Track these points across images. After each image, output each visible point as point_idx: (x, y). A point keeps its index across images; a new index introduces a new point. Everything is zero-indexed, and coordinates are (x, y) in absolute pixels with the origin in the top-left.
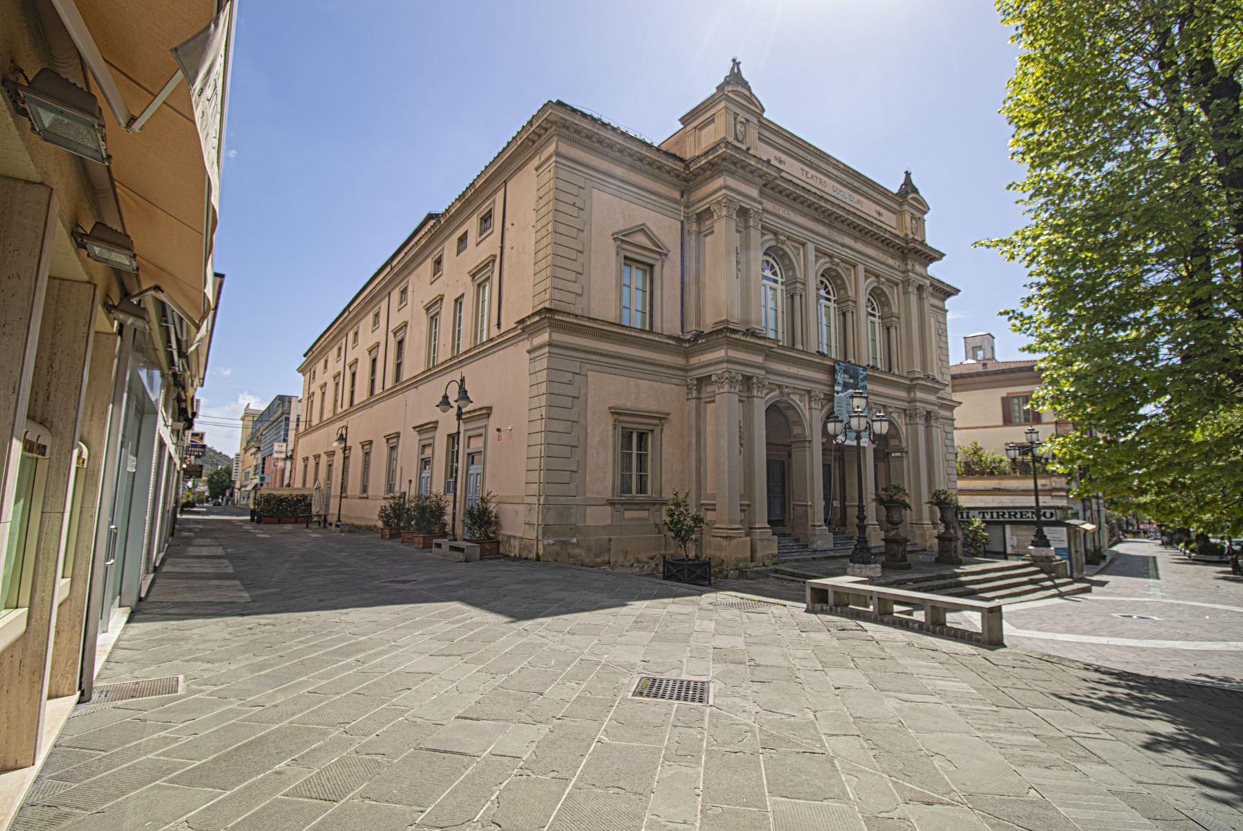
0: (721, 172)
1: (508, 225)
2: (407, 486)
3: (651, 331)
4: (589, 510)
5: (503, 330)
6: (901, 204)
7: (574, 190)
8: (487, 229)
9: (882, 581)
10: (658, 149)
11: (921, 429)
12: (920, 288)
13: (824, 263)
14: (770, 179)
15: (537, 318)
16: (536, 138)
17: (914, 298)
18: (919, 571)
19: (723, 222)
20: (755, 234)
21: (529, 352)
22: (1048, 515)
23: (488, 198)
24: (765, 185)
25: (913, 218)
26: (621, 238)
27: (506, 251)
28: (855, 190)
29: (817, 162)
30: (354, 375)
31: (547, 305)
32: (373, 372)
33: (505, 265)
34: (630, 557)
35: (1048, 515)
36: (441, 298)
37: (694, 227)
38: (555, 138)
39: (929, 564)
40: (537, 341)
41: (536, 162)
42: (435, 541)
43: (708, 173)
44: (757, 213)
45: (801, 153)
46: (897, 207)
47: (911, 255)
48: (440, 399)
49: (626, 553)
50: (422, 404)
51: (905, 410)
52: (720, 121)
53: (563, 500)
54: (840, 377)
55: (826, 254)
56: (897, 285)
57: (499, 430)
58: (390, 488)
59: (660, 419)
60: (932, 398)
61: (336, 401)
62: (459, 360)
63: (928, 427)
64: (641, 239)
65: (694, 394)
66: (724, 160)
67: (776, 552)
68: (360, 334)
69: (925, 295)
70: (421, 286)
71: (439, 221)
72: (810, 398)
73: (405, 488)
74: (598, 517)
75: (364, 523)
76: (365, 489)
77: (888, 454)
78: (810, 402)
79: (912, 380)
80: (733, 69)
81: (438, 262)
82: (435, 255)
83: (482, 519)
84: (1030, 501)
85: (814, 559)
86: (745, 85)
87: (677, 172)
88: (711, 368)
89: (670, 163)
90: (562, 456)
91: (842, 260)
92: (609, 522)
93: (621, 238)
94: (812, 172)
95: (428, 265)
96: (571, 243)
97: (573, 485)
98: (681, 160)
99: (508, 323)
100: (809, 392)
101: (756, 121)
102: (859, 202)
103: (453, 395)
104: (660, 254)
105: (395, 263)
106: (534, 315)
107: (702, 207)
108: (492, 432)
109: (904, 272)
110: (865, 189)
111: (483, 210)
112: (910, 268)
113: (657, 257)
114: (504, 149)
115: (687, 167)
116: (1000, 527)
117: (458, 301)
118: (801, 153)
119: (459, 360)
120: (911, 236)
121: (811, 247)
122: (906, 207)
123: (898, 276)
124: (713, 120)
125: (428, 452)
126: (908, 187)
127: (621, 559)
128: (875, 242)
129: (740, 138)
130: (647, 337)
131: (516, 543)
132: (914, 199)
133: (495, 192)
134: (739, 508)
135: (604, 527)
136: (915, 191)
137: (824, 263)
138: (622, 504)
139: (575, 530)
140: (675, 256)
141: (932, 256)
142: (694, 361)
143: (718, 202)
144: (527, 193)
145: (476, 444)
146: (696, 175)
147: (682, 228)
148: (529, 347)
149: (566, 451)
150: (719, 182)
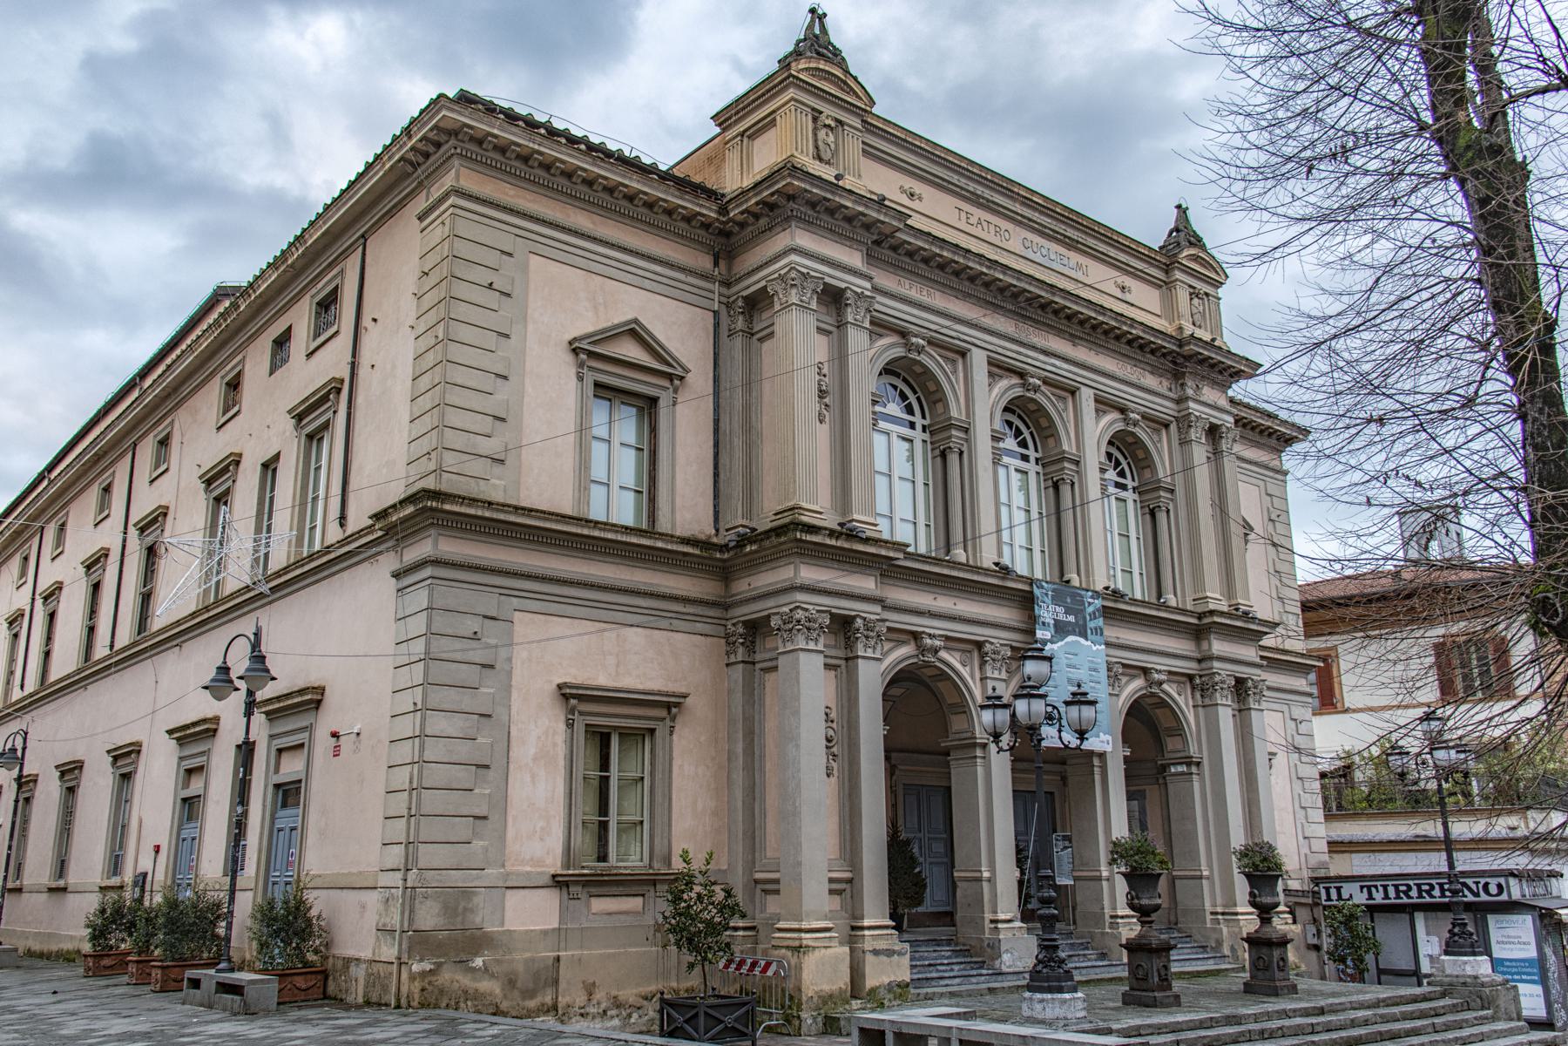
0: (787, 219)
1: (366, 321)
2: (149, 856)
3: (650, 533)
4: (513, 898)
5: (350, 529)
6: (1167, 269)
7: (492, 258)
8: (329, 325)
9: (1087, 1026)
10: (666, 177)
11: (1226, 716)
12: (1213, 432)
13: (1007, 388)
14: (888, 231)
15: (410, 510)
16: (431, 149)
17: (1200, 452)
18: (1192, 1008)
19: (795, 314)
20: (857, 339)
21: (397, 575)
22: (1493, 889)
23: (331, 266)
24: (877, 243)
25: (1194, 294)
26: (585, 351)
27: (363, 372)
28: (1071, 245)
29: (987, 193)
30: (52, 616)
31: (430, 483)
32: (93, 612)
33: (360, 400)
34: (599, 995)
35: (1493, 889)
36: (235, 461)
37: (740, 323)
38: (456, 162)
39: (1229, 995)
40: (413, 554)
41: (420, 203)
42: (191, 973)
43: (763, 221)
44: (860, 296)
45: (955, 178)
46: (1161, 275)
47: (1190, 367)
48: (213, 673)
49: (590, 990)
50: (178, 686)
51: (1191, 677)
52: (786, 122)
53: (456, 878)
54: (1048, 612)
55: (1011, 371)
56: (1167, 426)
57: (335, 735)
58: (116, 864)
59: (668, 706)
60: (1249, 652)
61: (11, 673)
62: (249, 600)
63: (1242, 712)
64: (629, 350)
65: (741, 654)
66: (791, 198)
67: (906, 976)
68: (69, 527)
69: (1224, 445)
70: (199, 438)
71: (235, 306)
72: (982, 656)
73: (145, 864)
74: (530, 915)
75: (54, 948)
76: (61, 867)
77: (1164, 768)
78: (983, 663)
79: (1200, 616)
80: (810, 27)
81: (234, 385)
82: (228, 372)
83: (289, 923)
84: (1435, 862)
85: (991, 990)
86: (836, 56)
87: (710, 223)
88: (770, 603)
89: (688, 204)
90: (450, 786)
91: (1046, 382)
92: (556, 925)
93: (585, 351)
94: (978, 213)
95: (214, 392)
96: (485, 361)
97: (478, 844)
98: (711, 194)
99: (358, 518)
100: (979, 645)
101: (857, 123)
102: (1079, 266)
103: (240, 663)
104: (670, 377)
105: (148, 382)
106: (403, 502)
107: (752, 285)
108: (322, 741)
109: (1178, 402)
110: (1091, 242)
111: (322, 289)
112: (1190, 392)
113: (666, 383)
114: (360, 176)
115: (723, 210)
116: (238, 894)
117: (270, 467)
118: (955, 178)
119: (249, 600)
120: (1187, 333)
121: (979, 359)
122: (1178, 275)
123: (1166, 408)
124: (773, 123)
125: (196, 786)
126: (1184, 233)
127: (581, 999)
128: (1113, 344)
129: (826, 155)
130: (640, 546)
131: (359, 972)
132: (1195, 258)
133: (345, 254)
134: (826, 886)
135: (545, 933)
136: (1196, 241)
137: (1007, 388)
138: (586, 884)
139: (477, 941)
140: (699, 379)
141: (1246, 369)
142: (742, 586)
143: (781, 278)
144: (399, 262)
145: (292, 767)
146: (742, 225)
147: (717, 325)
148: (396, 566)
149: (463, 776)
150: (781, 241)
